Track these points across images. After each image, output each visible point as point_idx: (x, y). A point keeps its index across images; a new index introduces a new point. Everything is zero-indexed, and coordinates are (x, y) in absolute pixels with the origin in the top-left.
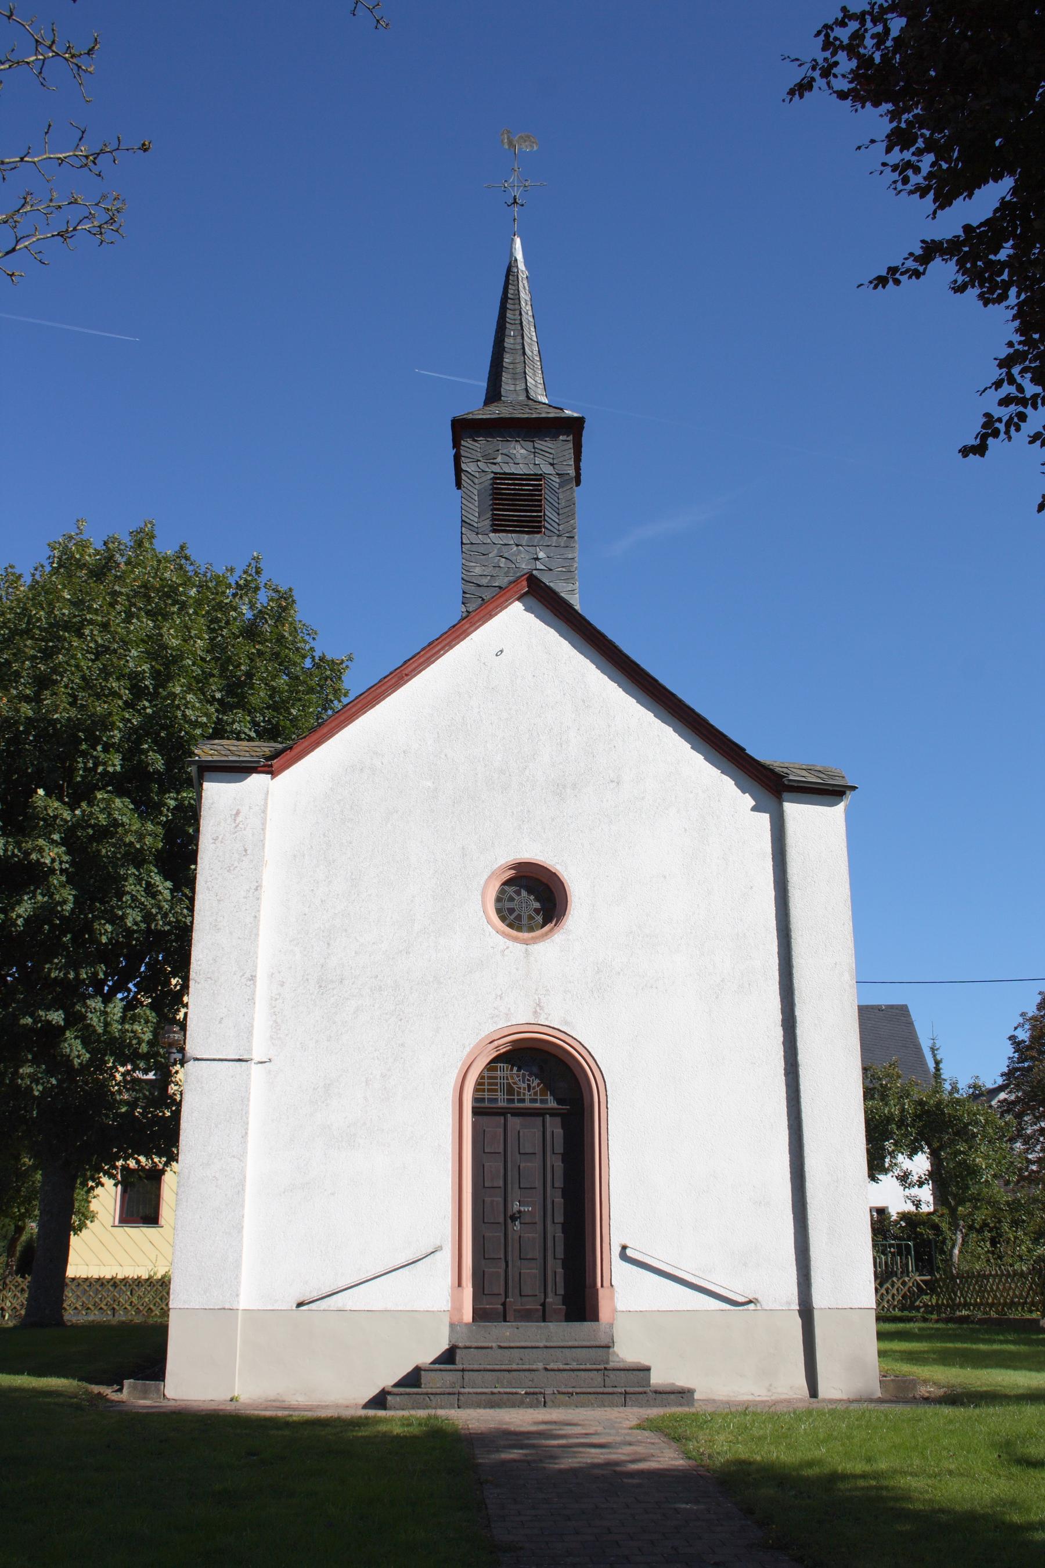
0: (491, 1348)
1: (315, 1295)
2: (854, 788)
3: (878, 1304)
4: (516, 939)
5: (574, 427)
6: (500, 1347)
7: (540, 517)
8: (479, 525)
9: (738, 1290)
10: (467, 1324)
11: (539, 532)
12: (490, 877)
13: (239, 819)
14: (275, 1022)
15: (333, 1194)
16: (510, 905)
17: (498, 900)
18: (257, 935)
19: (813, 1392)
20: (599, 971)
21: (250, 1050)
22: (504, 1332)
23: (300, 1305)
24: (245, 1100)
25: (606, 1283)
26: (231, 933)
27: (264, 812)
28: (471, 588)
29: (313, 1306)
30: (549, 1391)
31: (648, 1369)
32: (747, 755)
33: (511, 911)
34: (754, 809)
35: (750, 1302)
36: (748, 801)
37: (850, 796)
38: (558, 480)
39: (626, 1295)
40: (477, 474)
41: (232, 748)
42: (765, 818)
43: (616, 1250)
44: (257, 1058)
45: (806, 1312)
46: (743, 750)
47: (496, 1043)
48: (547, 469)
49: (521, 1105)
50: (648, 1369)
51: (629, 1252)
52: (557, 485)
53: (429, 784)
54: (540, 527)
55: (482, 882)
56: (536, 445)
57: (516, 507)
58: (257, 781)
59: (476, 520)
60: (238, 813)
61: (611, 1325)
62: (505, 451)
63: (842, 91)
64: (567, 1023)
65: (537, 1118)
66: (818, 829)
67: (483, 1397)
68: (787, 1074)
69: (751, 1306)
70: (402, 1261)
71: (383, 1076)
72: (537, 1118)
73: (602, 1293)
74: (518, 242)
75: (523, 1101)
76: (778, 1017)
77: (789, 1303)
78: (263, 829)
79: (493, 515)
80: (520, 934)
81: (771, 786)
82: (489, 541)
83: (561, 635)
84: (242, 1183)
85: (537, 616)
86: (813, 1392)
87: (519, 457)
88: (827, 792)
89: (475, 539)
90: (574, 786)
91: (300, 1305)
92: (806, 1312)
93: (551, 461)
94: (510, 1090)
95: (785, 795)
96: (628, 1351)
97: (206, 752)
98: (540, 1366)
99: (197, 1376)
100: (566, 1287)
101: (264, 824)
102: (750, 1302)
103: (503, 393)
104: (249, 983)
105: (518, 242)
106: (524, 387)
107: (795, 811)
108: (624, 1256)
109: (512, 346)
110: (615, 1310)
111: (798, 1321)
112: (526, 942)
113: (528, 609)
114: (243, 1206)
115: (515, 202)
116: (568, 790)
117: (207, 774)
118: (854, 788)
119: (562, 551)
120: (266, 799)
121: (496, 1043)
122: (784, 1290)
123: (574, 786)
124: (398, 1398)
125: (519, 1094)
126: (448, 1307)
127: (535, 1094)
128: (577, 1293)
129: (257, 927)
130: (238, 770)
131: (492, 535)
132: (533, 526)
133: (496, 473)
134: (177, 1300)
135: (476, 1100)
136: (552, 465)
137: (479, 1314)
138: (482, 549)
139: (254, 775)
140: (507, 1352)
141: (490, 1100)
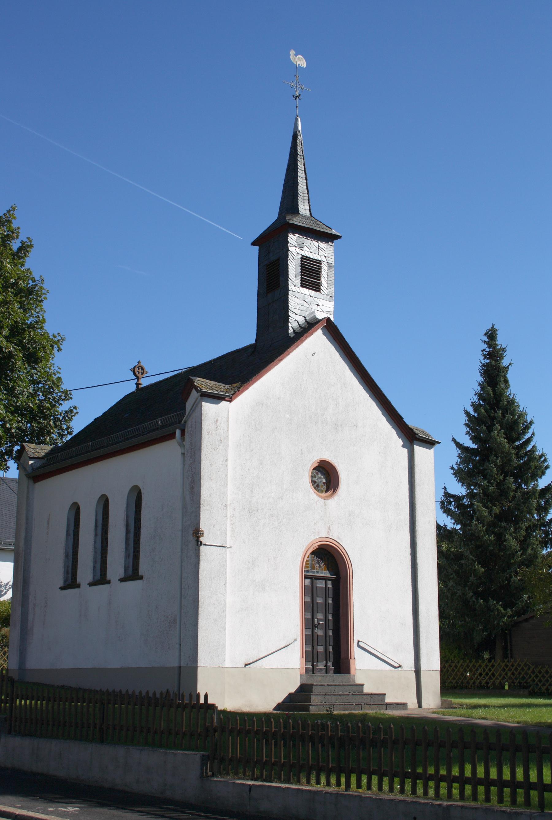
0: (324, 685)
1: (251, 661)
2: (439, 443)
6: (328, 685)
11: (318, 291)
13: (218, 424)
14: (232, 528)
15: (257, 613)
18: (227, 484)
19: (420, 705)
20: (350, 516)
21: (226, 542)
23: (246, 665)
24: (225, 566)
25: (353, 657)
26: (216, 482)
27: (228, 421)
29: (250, 666)
30: (363, 704)
31: (384, 695)
32: (403, 421)
34: (403, 446)
36: (400, 442)
37: (437, 446)
43: (356, 643)
45: (418, 672)
46: (402, 418)
48: (324, 259)
50: (384, 695)
51: (361, 644)
53: (288, 416)
58: (224, 403)
60: (217, 421)
64: (339, 538)
67: (342, 706)
68: (412, 568)
70: (283, 646)
71: (274, 558)
73: (352, 661)
76: (409, 542)
77: (411, 668)
78: (228, 430)
81: (411, 437)
83: (336, 350)
84: (225, 607)
85: (327, 338)
86: (420, 705)
88: (429, 443)
90: (341, 425)
91: (246, 665)
92: (418, 672)
95: (415, 442)
99: (366, 690)
100: (333, 660)
101: (228, 428)
104: (225, 508)
108: (359, 646)
110: (356, 669)
111: (414, 676)
112: (325, 498)
113: (324, 334)
114: (225, 618)
116: (339, 428)
118: (439, 443)
120: (228, 415)
122: (409, 663)
123: (341, 425)
124: (313, 707)
128: (341, 662)
129: (227, 480)
130: (217, 398)
131: (301, 288)
133: (302, 256)
136: (325, 257)
139: (223, 402)
140: (330, 687)
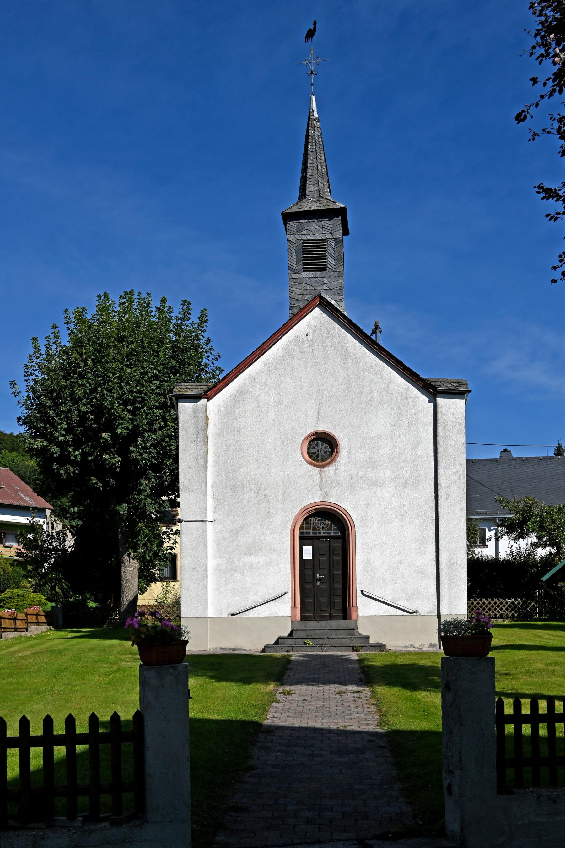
3: (469, 612)
4: (315, 466)
5: (342, 213)
7: (326, 262)
8: (297, 268)
9: (410, 607)
10: (298, 621)
12: (304, 439)
16: (313, 451)
17: (308, 448)
22: (312, 624)
28: (294, 302)
29: (237, 616)
33: (314, 453)
35: (414, 612)
38: (334, 242)
39: (364, 608)
40: (294, 241)
41: (189, 387)
42: (432, 404)
44: (209, 520)
47: (308, 510)
48: (328, 236)
49: (320, 535)
52: (334, 244)
54: (326, 267)
55: (301, 442)
56: (323, 224)
57: (313, 257)
59: (295, 266)
61: (356, 621)
62: (308, 228)
63: (119, 717)
65: (327, 540)
66: (453, 409)
69: (415, 614)
72: (327, 540)
74: (314, 98)
75: (320, 533)
79: (303, 263)
80: (318, 463)
81: (432, 390)
82: (301, 276)
87: (316, 230)
89: (294, 276)
93: (330, 231)
94: (315, 529)
96: (362, 631)
97: (178, 390)
98: (326, 637)
102: (414, 612)
103: (307, 192)
105: (314, 98)
106: (317, 188)
107: (441, 401)
109: (311, 165)
110: (357, 615)
112: (321, 467)
115: (312, 73)
117: (179, 400)
119: (336, 279)
121: (308, 510)
125: (319, 530)
126: (290, 615)
127: (326, 530)
132: (321, 267)
133: (304, 240)
134: (185, 612)
135: (300, 533)
136: (331, 233)
137: (303, 618)
138: (298, 281)
141: (307, 533)
